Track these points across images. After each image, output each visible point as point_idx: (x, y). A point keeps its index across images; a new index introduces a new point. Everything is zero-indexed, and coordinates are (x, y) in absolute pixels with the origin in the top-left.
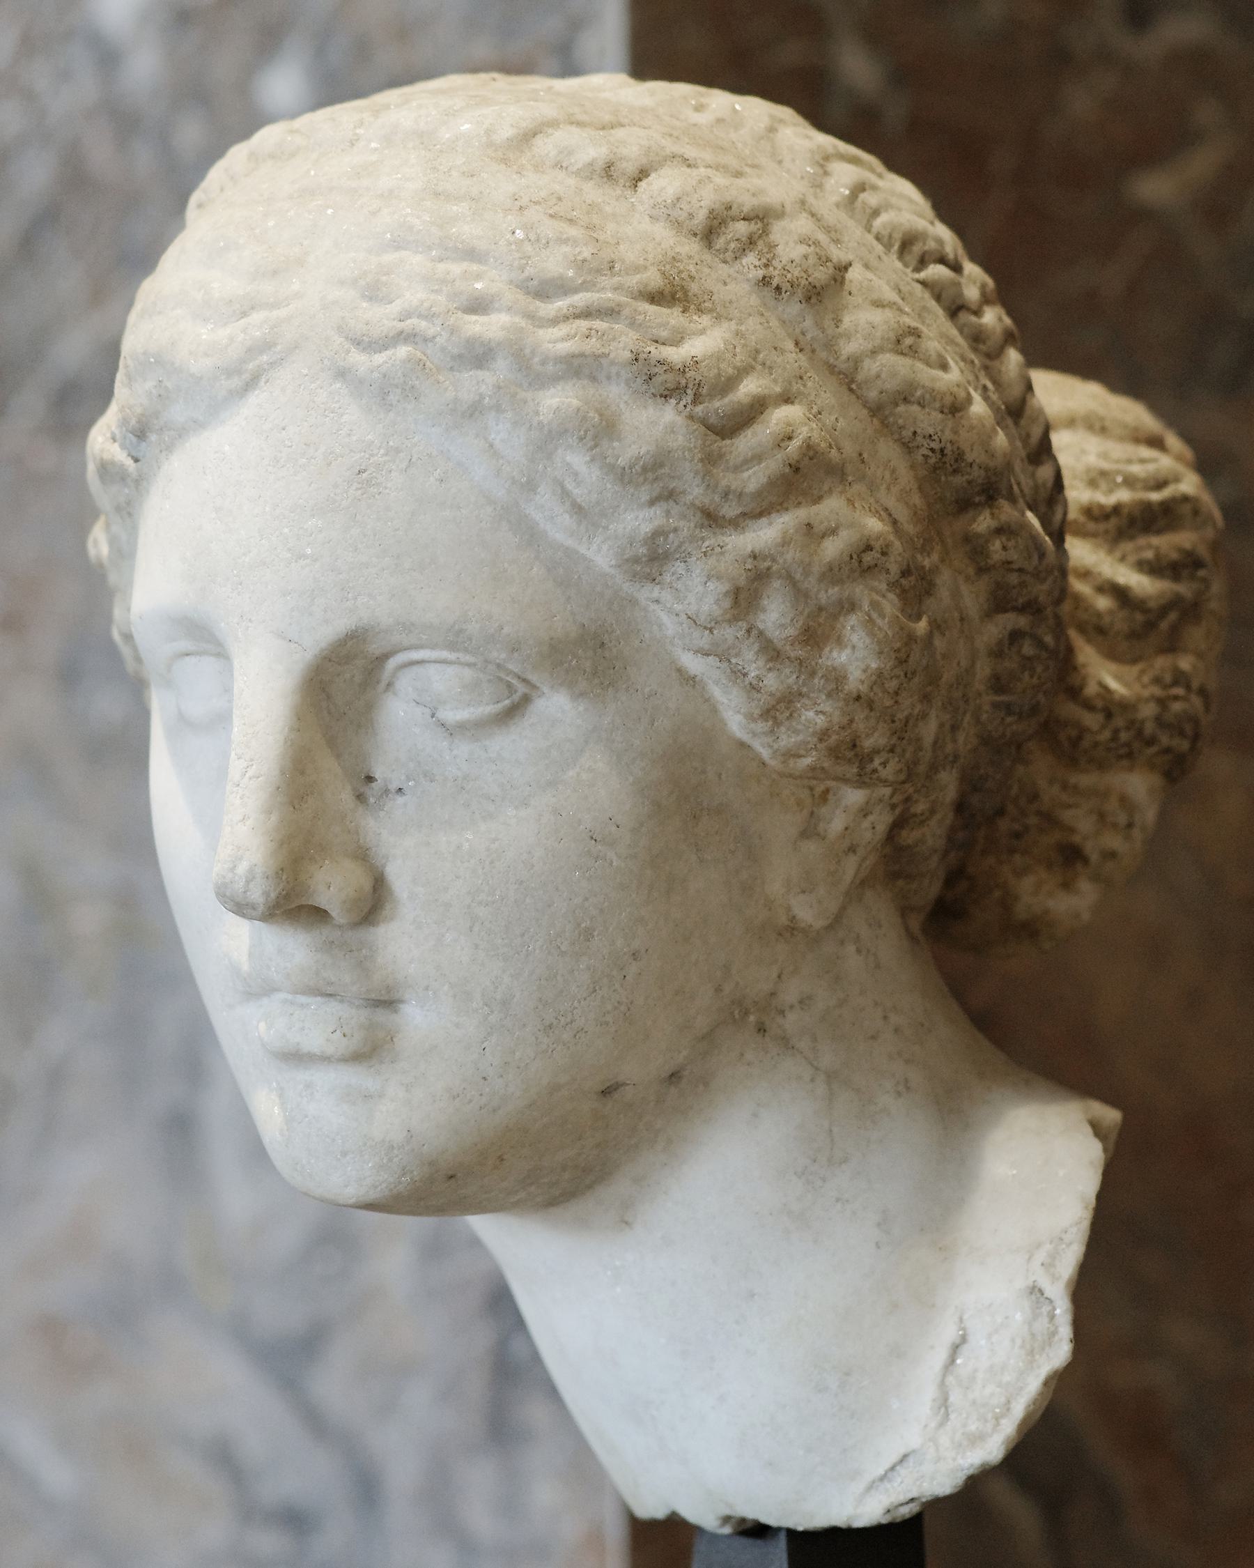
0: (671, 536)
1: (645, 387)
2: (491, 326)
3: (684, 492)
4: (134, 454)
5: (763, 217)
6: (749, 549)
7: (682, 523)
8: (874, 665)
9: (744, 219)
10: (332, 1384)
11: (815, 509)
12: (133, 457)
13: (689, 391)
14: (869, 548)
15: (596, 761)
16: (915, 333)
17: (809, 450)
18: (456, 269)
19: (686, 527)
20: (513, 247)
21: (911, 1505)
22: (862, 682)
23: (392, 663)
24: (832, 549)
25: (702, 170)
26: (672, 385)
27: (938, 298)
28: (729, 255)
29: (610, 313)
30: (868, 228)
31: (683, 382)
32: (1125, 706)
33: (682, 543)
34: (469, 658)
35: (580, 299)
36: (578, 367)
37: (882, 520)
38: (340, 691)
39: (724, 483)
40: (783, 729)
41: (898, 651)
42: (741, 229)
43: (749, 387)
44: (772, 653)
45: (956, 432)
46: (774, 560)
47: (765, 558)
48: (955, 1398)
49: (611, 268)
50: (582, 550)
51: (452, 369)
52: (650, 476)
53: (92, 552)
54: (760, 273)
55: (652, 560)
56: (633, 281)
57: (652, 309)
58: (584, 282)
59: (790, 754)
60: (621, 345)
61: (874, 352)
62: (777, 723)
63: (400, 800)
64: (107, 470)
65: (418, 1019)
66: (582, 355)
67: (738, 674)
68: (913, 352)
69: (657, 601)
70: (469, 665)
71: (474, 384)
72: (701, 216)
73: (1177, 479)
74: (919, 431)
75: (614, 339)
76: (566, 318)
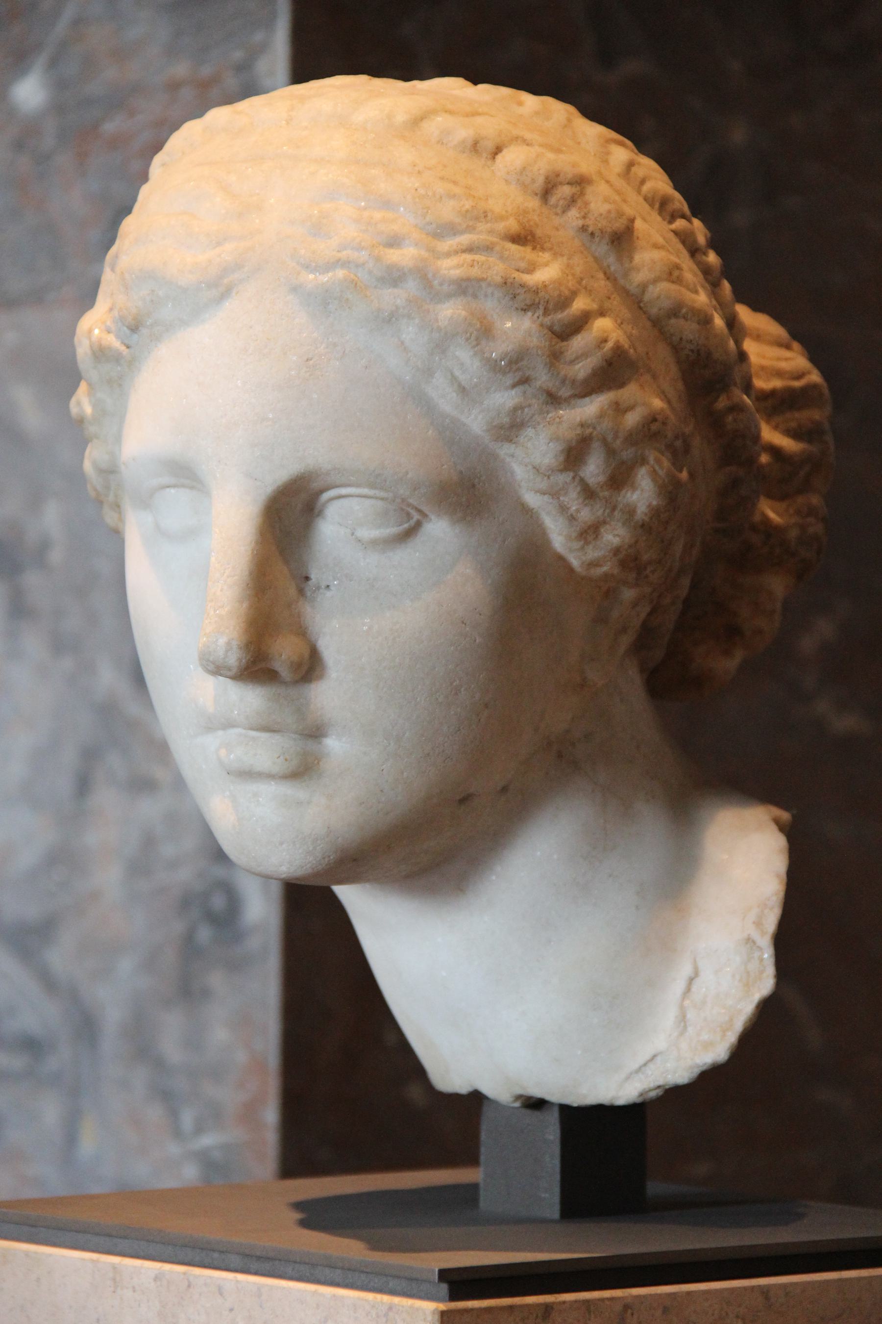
0: (526, 410)
1: (511, 303)
2: (405, 255)
3: (535, 379)
4: (126, 342)
5: (581, 182)
6: (578, 419)
7: (534, 401)
8: (655, 503)
9: (568, 183)
10: (59, 957)
11: (621, 392)
12: (125, 344)
13: (541, 306)
14: (655, 420)
15: (466, 569)
16: (678, 267)
17: (618, 350)
18: (378, 215)
19: (536, 404)
20: (417, 200)
21: (658, 1091)
22: (646, 514)
23: (326, 496)
24: (632, 419)
25: (537, 147)
26: (529, 300)
27: (683, 242)
28: (559, 210)
29: (488, 248)
30: (639, 192)
31: (537, 300)
32: (778, 530)
33: (533, 415)
34: (382, 494)
35: (465, 239)
36: (465, 287)
37: (662, 400)
38: (289, 517)
39: (563, 373)
40: (591, 547)
41: (670, 492)
42: (566, 191)
43: (580, 304)
44: (589, 493)
45: (707, 338)
46: (594, 428)
47: (588, 427)
48: (691, 1015)
49: (485, 217)
50: (463, 418)
51: (375, 287)
52: (514, 367)
53: (74, 409)
54: (580, 223)
55: (511, 428)
56: (501, 226)
57: (514, 247)
58: (468, 226)
59: (593, 564)
60: (495, 272)
61: (655, 281)
62: (587, 543)
63: (329, 594)
64: (101, 354)
65: (335, 745)
66: (468, 279)
67: (563, 509)
68: (679, 281)
69: (513, 456)
70: (382, 499)
71: (392, 298)
72: (540, 181)
73: (809, 373)
74: (684, 337)
75: (489, 268)
76: (456, 252)
